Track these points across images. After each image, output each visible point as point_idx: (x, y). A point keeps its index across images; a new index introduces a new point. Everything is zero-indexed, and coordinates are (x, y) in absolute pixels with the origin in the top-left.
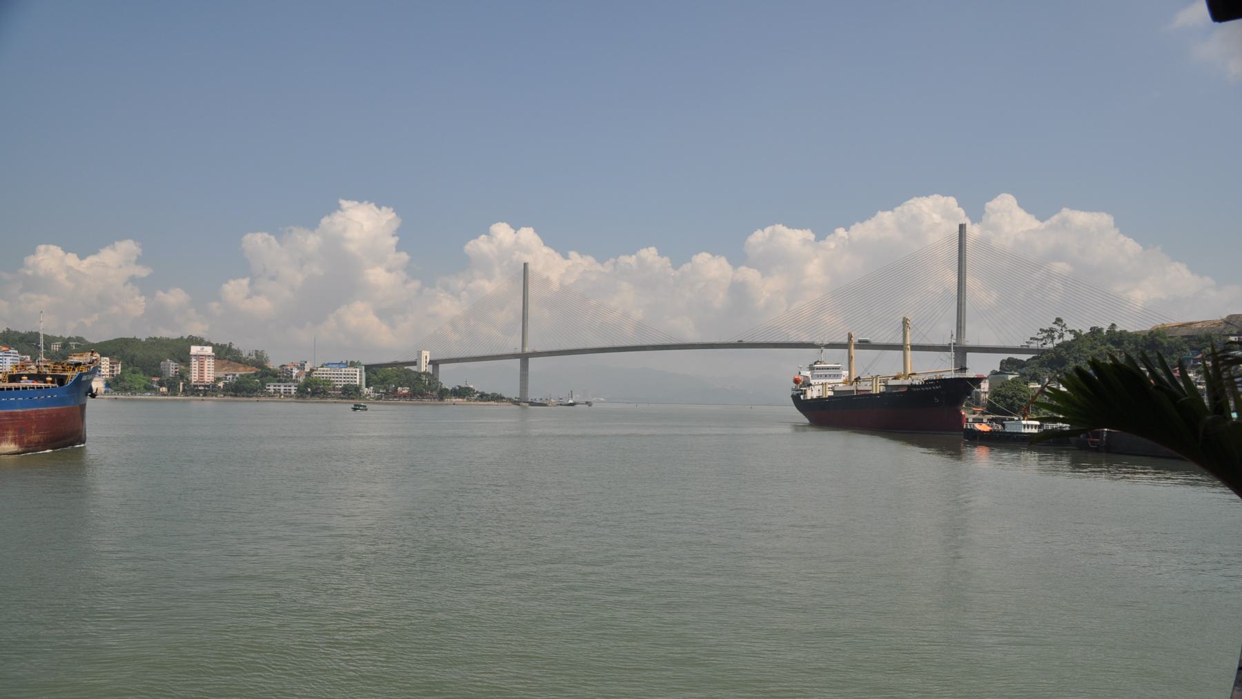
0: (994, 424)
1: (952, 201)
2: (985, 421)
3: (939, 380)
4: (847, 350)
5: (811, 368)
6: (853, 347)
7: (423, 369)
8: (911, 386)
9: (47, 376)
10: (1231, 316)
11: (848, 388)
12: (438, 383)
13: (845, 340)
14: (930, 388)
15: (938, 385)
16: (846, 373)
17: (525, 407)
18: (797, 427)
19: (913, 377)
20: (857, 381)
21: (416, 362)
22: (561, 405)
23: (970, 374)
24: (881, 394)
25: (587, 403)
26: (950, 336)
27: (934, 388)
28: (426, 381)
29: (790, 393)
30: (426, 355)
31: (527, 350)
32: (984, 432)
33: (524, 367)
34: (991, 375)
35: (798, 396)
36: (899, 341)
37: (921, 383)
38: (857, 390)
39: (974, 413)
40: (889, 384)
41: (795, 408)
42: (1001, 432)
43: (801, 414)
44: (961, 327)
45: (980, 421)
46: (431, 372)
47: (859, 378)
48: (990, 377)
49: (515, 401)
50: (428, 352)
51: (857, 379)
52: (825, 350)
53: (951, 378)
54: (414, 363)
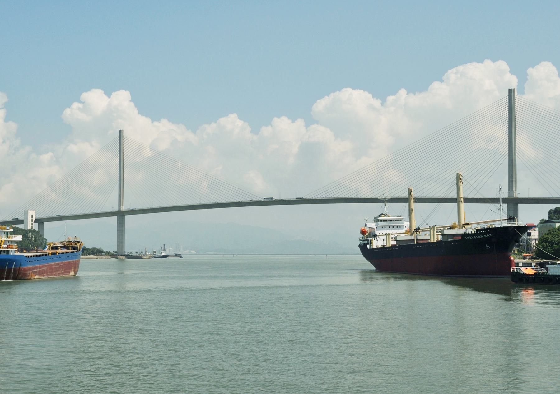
0: (539, 268)
1: (503, 65)
2: (534, 264)
3: (489, 229)
4: (408, 204)
5: (376, 220)
6: (412, 200)
7: (29, 227)
8: (466, 235)
9: (70, 247)
10: (556, 207)
11: (409, 238)
12: (43, 239)
13: (406, 195)
14: (482, 236)
15: (489, 233)
16: (407, 224)
17: (122, 260)
18: (365, 274)
19: (467, 226)
20: (416, 231)
21: (23, 221)
22: (155, 257)
23: (521, 222)
24: (438, 242)
25: (176, 255)
26: (499, 189)
27: (485, 236)
28: (32, 237)
29: (358, 243)
30: (33, 214)
31: (124, 208)
32: (529, 275)
33: (121, 224)
34: (540, 223)
35: (365, 245)
36: (453, 195)
37: (473, 232)
38: (417, 239)
39: (524, 258)
40: (445, 233)
41: (362, 256)
42: (545, 275)
43: (368, 262)
44: (512, 181)
45: (526, 265)
46: (37, 230)
47: (419, 228)
48: (539, 226)
49: (113, 255)
50: (34, 211)
51: (417, 230)
52: (388, 204)
53: (501, 227)
54: (21, 222)
